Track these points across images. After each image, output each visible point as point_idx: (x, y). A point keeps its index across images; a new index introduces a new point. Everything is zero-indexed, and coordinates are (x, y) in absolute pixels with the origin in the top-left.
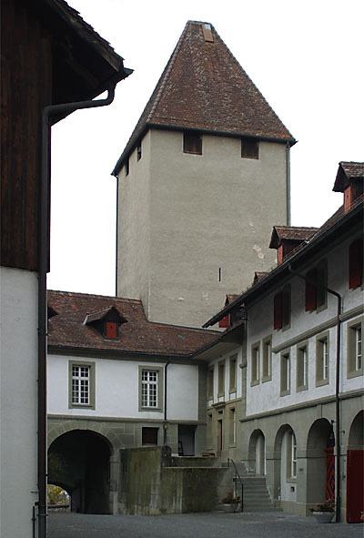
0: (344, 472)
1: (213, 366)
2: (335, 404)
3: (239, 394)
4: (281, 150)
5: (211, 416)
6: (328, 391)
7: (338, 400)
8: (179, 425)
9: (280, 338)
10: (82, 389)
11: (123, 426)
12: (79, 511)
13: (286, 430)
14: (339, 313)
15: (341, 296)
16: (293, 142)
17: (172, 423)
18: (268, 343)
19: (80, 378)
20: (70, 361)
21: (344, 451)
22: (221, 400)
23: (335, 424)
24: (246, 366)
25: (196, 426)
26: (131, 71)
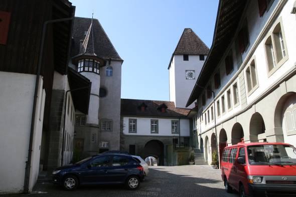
6: (212, 124)
13: (207, 138)
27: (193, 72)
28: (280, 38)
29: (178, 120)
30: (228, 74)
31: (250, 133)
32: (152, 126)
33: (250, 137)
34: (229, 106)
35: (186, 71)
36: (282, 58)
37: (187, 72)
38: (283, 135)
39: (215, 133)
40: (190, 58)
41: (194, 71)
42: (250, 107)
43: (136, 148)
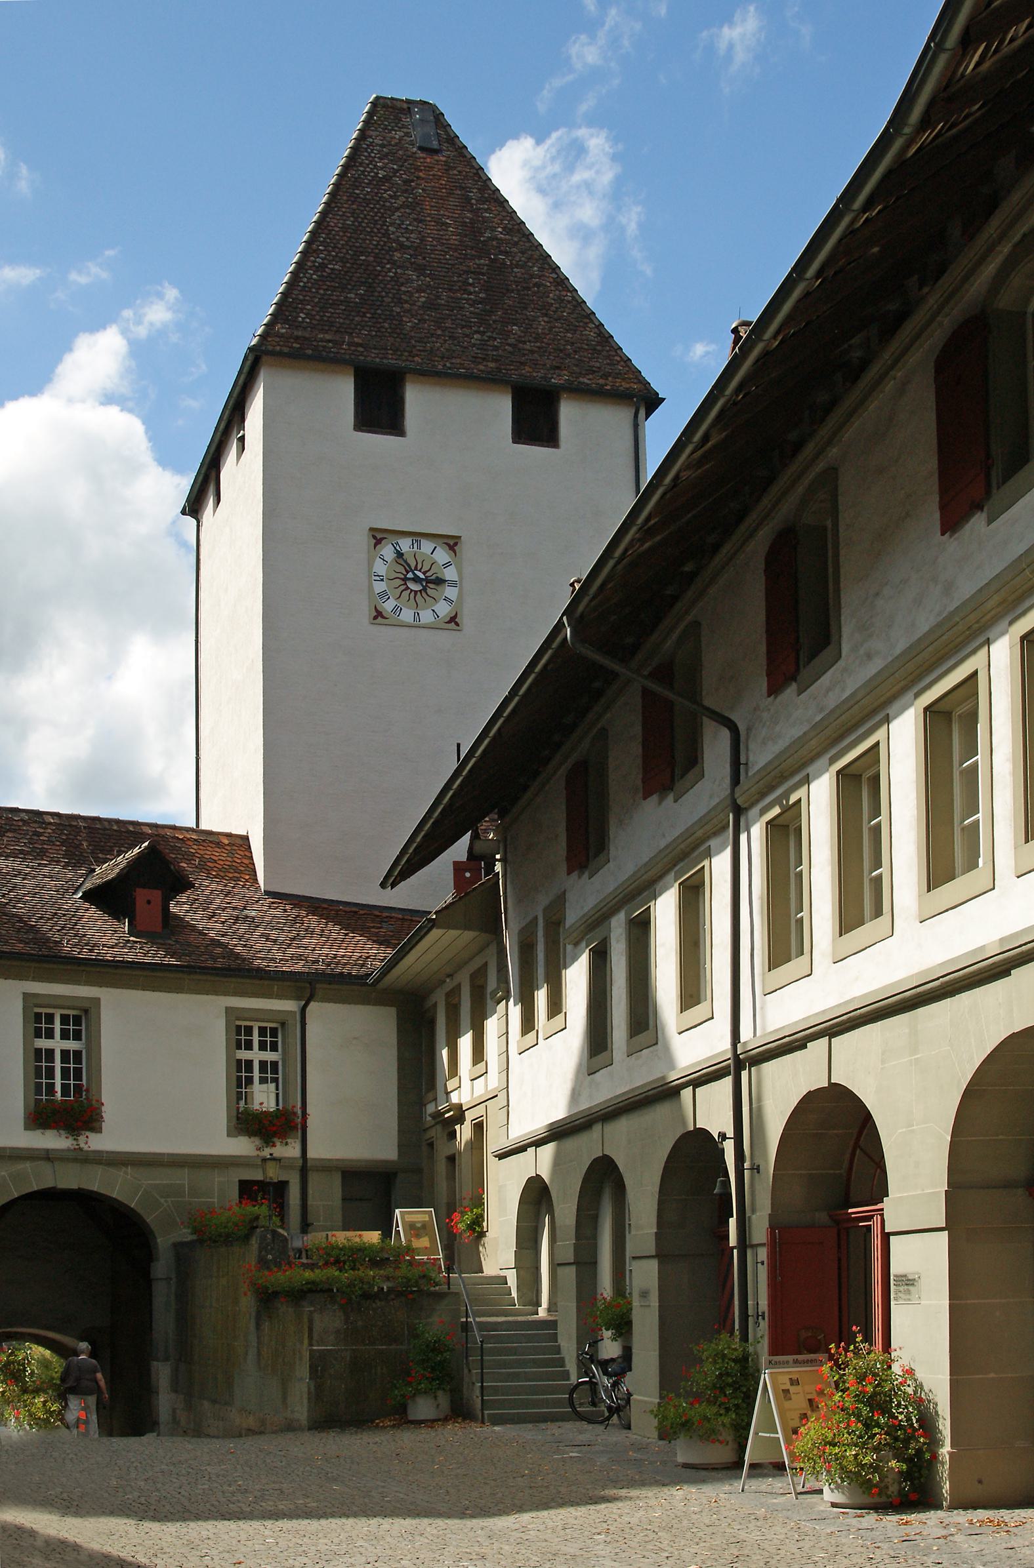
0: (761, 1298)
1: (435, 1005)
2: (727, 1083)
5: (431, 1145)
11: (182, 1178)
14: (736, 780)
15: (742, 728)
17: (326, 1167)
19: (58, 1044)
20: (26, 996)
21: (760, 1231)
23: (729, 1147)
25: (395, 1174)
29: (289, 1006)
35: (378, 537)
41: (452, 543)
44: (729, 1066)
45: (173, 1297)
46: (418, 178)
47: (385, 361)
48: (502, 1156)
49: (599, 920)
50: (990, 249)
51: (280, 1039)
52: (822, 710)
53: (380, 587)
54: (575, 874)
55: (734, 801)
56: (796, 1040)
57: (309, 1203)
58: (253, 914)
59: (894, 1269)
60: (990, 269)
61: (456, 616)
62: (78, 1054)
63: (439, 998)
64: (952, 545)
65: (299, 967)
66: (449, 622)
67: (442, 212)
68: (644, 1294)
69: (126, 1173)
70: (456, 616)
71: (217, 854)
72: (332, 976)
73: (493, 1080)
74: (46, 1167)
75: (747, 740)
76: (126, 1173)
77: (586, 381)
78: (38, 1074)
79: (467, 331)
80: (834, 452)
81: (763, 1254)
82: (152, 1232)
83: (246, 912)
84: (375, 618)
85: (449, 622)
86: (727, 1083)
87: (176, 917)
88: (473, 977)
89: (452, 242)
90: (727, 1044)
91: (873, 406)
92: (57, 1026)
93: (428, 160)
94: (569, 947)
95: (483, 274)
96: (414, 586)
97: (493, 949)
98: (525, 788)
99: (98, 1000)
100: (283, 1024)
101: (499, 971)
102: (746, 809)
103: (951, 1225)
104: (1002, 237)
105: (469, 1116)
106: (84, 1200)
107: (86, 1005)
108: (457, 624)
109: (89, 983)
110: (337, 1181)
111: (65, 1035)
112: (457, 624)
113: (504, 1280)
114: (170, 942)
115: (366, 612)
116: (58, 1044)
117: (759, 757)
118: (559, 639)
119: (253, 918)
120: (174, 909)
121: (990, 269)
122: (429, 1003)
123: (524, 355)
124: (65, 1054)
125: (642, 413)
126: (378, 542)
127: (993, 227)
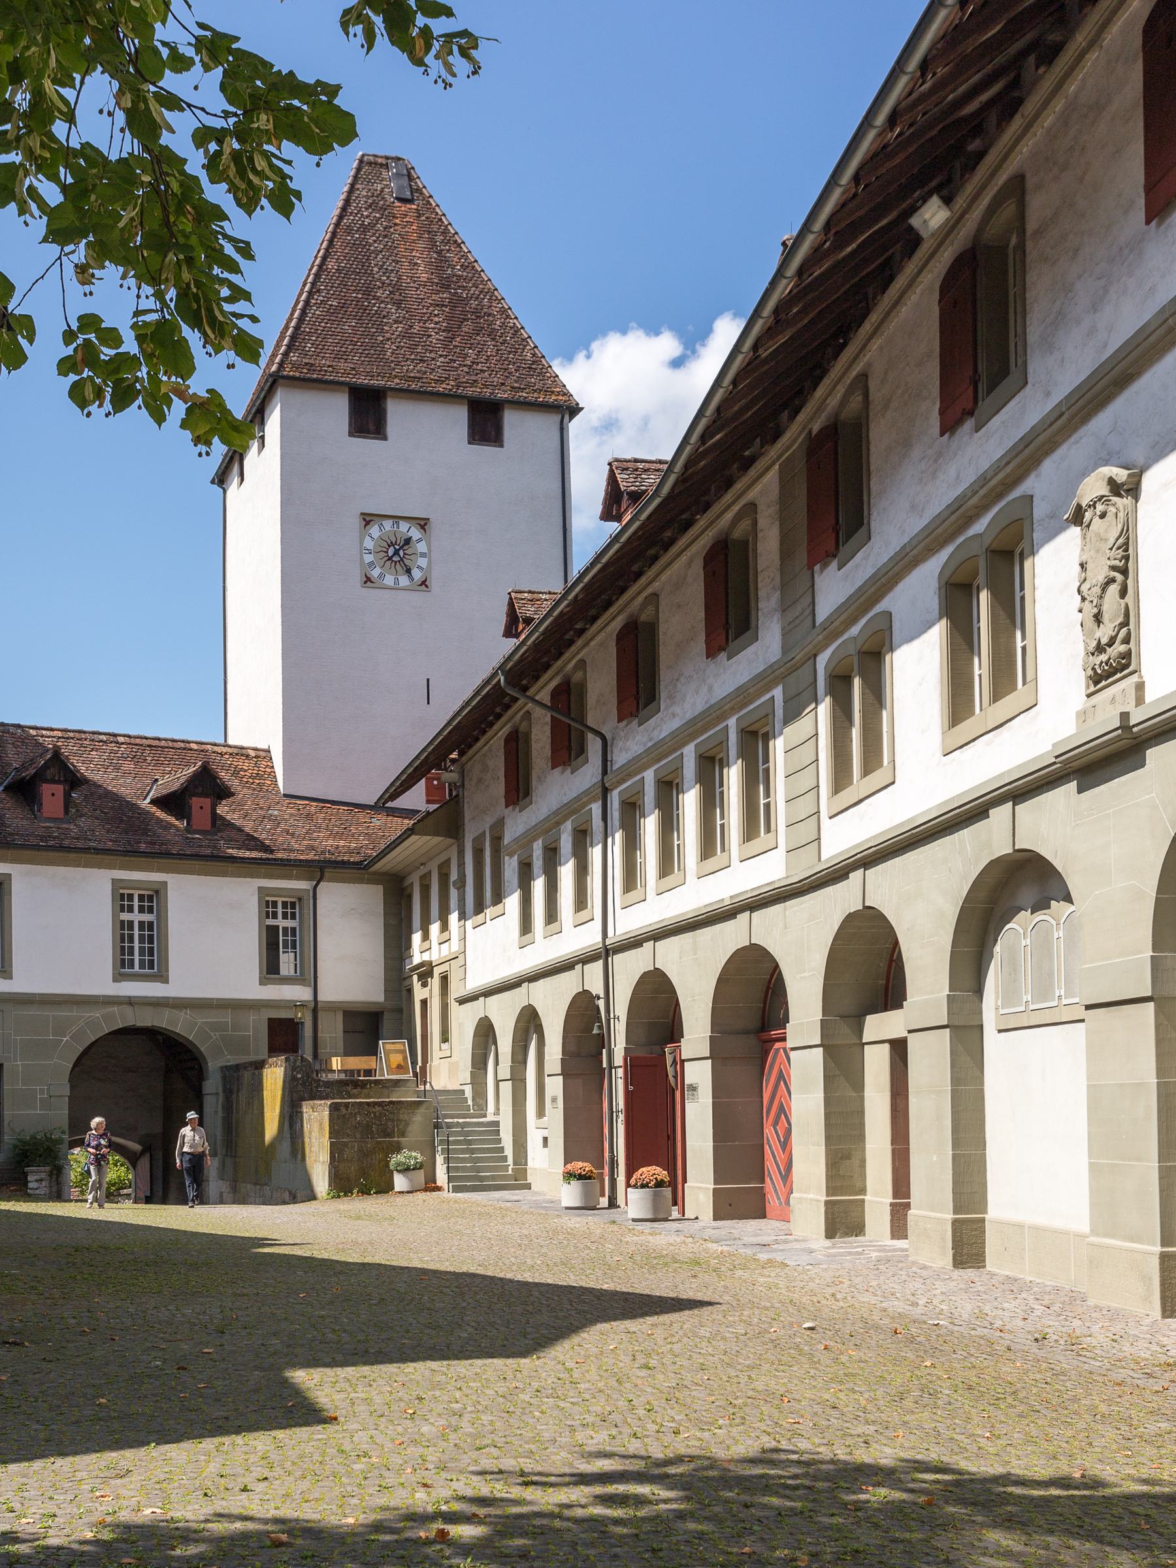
2: (600, 963)
3: (455, 946)
4: (550, 422)
6: (588, 937)
7: (605, 953)
8: (344, 1012)
9: (517, 824)
10: (131, 938)
11: (227, 1017)
12: (149, 1200)
13: (530, 1022)
14: (605, 772)
15: (608, 737)
16: (574, 410)
17: (332, 1007)
18: (497, 839)
22: (426, 957)
24: (464, 886)
26: (583, 408)
27: (415, 533)
28: (1019, 634)
29: (303, 885)
30: (711, 653)
31: (825, 1011)
32: (123, 931)
33: (825, 1026)
34: (709, 844)
35: (368, 519)
36: (1014, 688)
37: (375, 530)
38: (982, 1026)
39: (597, 988)
40: (397, 412)
41: (423, 524)
42: (836, 875)
43: (641, 1053)
44: (601, 952)
45: (220, 1107)
46: (396, 224)
47: (372, 382)
48: (462, 1001)
49: (525, 841)
50: (729, 507)
51: (297, 910)
52: (650, 740)
53: (368, 558)
54: (510, 808)
55: (603, 784)
56: (638, 940)
57: (319, 1035)
58: (276, 813)
59: (687, 1082)
60: (729, 515)
61: (426, 580)
62: (151, 924)
63: (415, 880)
64: (712, 667)
65: (311, 856)
66: (421, 585)
67: (414, 254)
68: (554, 1100)
69: (186, 1013)
70: (426, 580)
71: (246, 765)
72: (336, 862)
73: (455, 946)
74: (128, 1010)
75: (612, 744)
76: (186, 1013)
77: (524, 395)
78: (123, 941)
79: (433, 355)
80: (657, 584)
81: (620, 1072)
82: (205, 1059)
83: (270, 812)
84: (365, 582)
85: (421, 585)
86: (600, 963)
87: (222, 818)
88: (440, 867)
89: (422, 279)
90: (599, 938)
91: (676, 566)
92: (136, 903)
93: (403, 209)
94: (507, 858)
95: (446, 306)
96: (391, 551)
97: (455, 849)
98: (477, 739)
99: (166, 883)
100: (300, 899)
101: (459, 866)
102: (611, 790)
103: (712, 1057)
104: (733, 503)
105: (437, 971)
106: (151, 1033)
107: (156, 887)
108: (427, 586)
109: (160, 870)
110: (340, 1017)
111: (141, 910)
112: (427, 586)
113: (463, 1092)
114: (216, 837)
115: (358, 578)
116: (136, 917)
117: (620, 758)
118: (496, 680)
119: (276, 816)
120: (219, 811)
121: (729, 515)
122: (406, 883)
123: (477, 374)
124: (141, 924)
125: (567, 417)
126: (367, 523)
127: (729, 497)
